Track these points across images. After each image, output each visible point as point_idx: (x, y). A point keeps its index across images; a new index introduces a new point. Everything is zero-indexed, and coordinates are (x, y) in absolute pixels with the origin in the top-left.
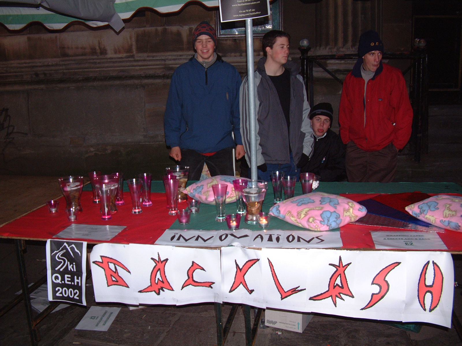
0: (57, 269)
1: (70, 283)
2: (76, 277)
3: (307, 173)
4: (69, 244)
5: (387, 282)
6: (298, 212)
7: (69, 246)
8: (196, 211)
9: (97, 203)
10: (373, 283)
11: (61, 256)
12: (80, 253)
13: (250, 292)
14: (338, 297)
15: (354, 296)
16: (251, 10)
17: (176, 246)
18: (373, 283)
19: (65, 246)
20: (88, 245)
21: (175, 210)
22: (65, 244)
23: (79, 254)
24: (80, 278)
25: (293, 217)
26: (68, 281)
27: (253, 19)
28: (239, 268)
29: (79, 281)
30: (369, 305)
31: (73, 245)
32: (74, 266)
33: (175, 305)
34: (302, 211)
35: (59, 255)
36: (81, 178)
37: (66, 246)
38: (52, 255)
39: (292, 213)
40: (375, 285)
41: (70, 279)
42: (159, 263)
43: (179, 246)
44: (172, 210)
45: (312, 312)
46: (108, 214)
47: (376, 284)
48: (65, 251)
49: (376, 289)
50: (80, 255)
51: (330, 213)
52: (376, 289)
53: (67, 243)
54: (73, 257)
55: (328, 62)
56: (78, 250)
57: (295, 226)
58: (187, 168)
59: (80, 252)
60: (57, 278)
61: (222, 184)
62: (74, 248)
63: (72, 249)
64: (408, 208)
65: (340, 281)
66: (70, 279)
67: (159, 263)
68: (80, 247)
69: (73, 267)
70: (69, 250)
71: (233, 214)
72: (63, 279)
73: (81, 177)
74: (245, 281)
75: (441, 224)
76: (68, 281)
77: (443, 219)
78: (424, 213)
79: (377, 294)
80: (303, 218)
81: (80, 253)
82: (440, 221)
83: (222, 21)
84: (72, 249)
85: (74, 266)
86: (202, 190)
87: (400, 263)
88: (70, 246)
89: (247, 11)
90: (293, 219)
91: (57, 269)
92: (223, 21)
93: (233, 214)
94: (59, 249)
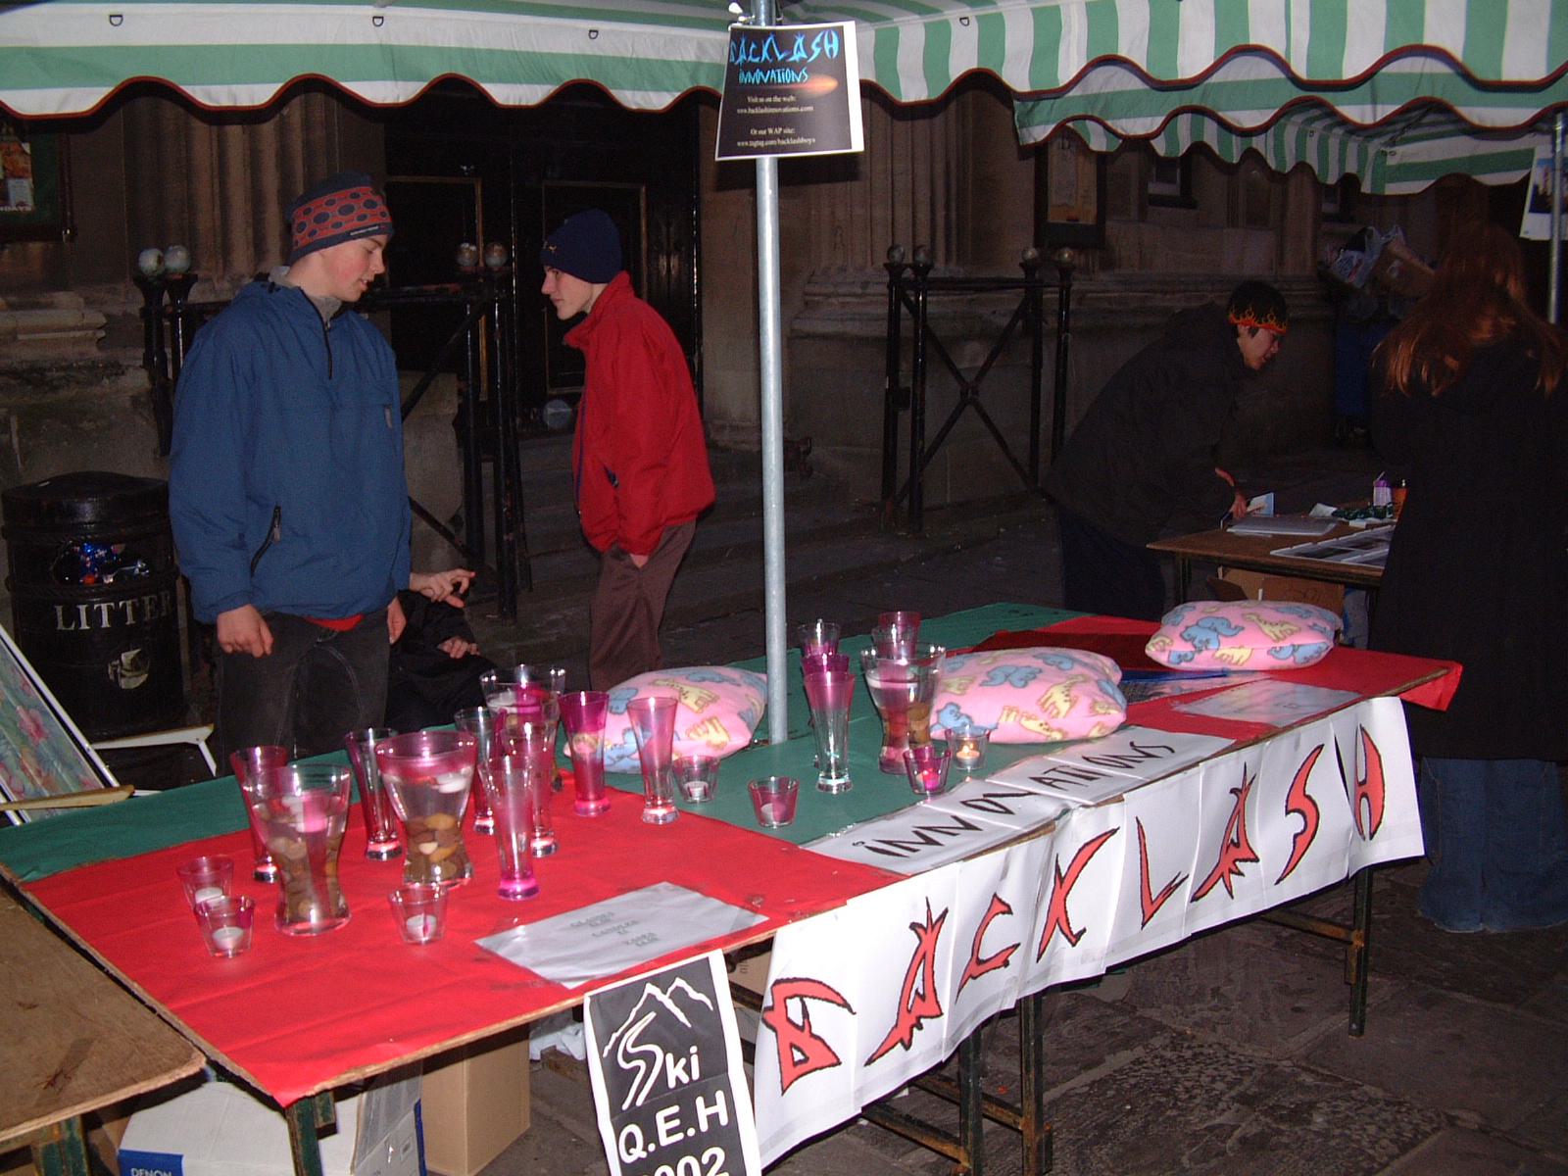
0: (625, 1107)
1: (680, 1136)
2: (675, 1109)
3: (899, 613)
4: (662, 982)
5: (1309, 797)
6: (1039, 700)
7: (665, 993)
8: (705, 793)
9: (272, 881)
10: (1287, 813)
11: (633, 1046)
12: (708, 1002)
13: (1074, 940)
14: (1233, 873)
15: (1259, 857)
16: (781, 129)
17: (965, 859)
18: (1287, 813)
19: (651, 996)
20: (727, 957)
21: (664, 805)
22: (650, 989)
23: (707, 1007)
24: (720, 1095)
25: (1029, 718)
26: (670, 1133)
27: (780, 160)
28: (1060, 874)
29: (721, 1108)
30: (830, 995)
31: (679, 982)
32: (695, 1060)
33: (941, 1062)
34: (1047, 696)
35: (625, 1047)
36: (465, 746)
37: (654, 997)
38: (605, 1054)
39: (1021, 711)
40: (1292, 814)
41: (676, 1123)
42: (926, 933)
43: (989, 846)
44: (655, 806)
45: (1193, 934)
46: (524, 877)
47: (1294, 811)
48: (652, 1015)
49: (1296, 823)
50: (712, 1008)
51: (941, 714)
52: (1296, 823)
53: (654, 980)
54: (689, 1025)
55: (1045, 289)
56: (698, 992)
57: (1028, 744)
58: (490, 677)
59: (708, 997)
60: (631, 1142)
61: (657, 698)
62: (682, 989)
63: (679, 997)
64: (1153, 645)
65: (1386, 788)
66: (676, 1123)
67: (926, 933)
68: (701, 976)
69: (687, 1069)
70: (670, 1005)
71: (773, 779)
72: (651, 1135)
73: (385, 753)
74: (1066, 912)
75: (1273, 659)
76: (670, 1133)
77: (1274, 645)
78: (1210, 646)
79: (1302, 832)
80: (1067, 712)
81: (708, 1002)
82: (1269, 652)
83: (717, 159)
84: (679, 997)
85: (695, 1060)
86: (1192, 626)
87: (1323, 745)
88: (670, 989)
89: (770, 131)
90: (1033, 725)
91: (625, 1107)
92: (719, 156)
93: (773, 779)
94: (628, 1019)
